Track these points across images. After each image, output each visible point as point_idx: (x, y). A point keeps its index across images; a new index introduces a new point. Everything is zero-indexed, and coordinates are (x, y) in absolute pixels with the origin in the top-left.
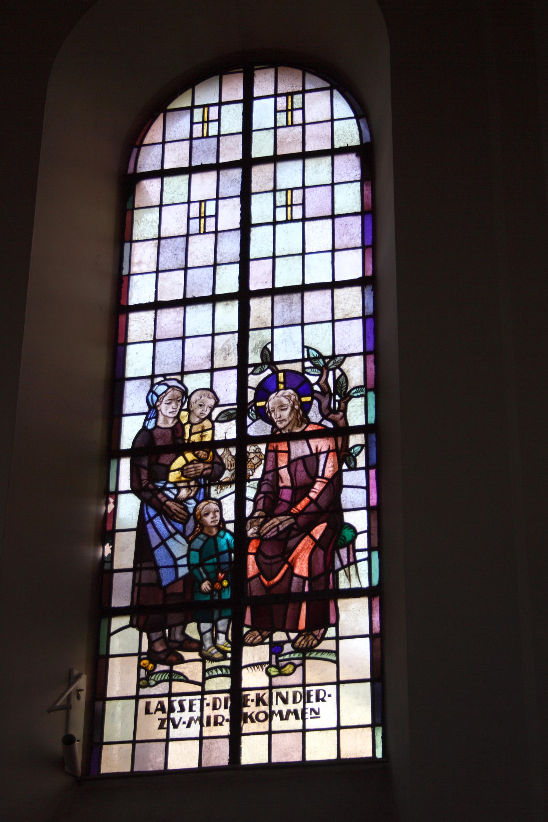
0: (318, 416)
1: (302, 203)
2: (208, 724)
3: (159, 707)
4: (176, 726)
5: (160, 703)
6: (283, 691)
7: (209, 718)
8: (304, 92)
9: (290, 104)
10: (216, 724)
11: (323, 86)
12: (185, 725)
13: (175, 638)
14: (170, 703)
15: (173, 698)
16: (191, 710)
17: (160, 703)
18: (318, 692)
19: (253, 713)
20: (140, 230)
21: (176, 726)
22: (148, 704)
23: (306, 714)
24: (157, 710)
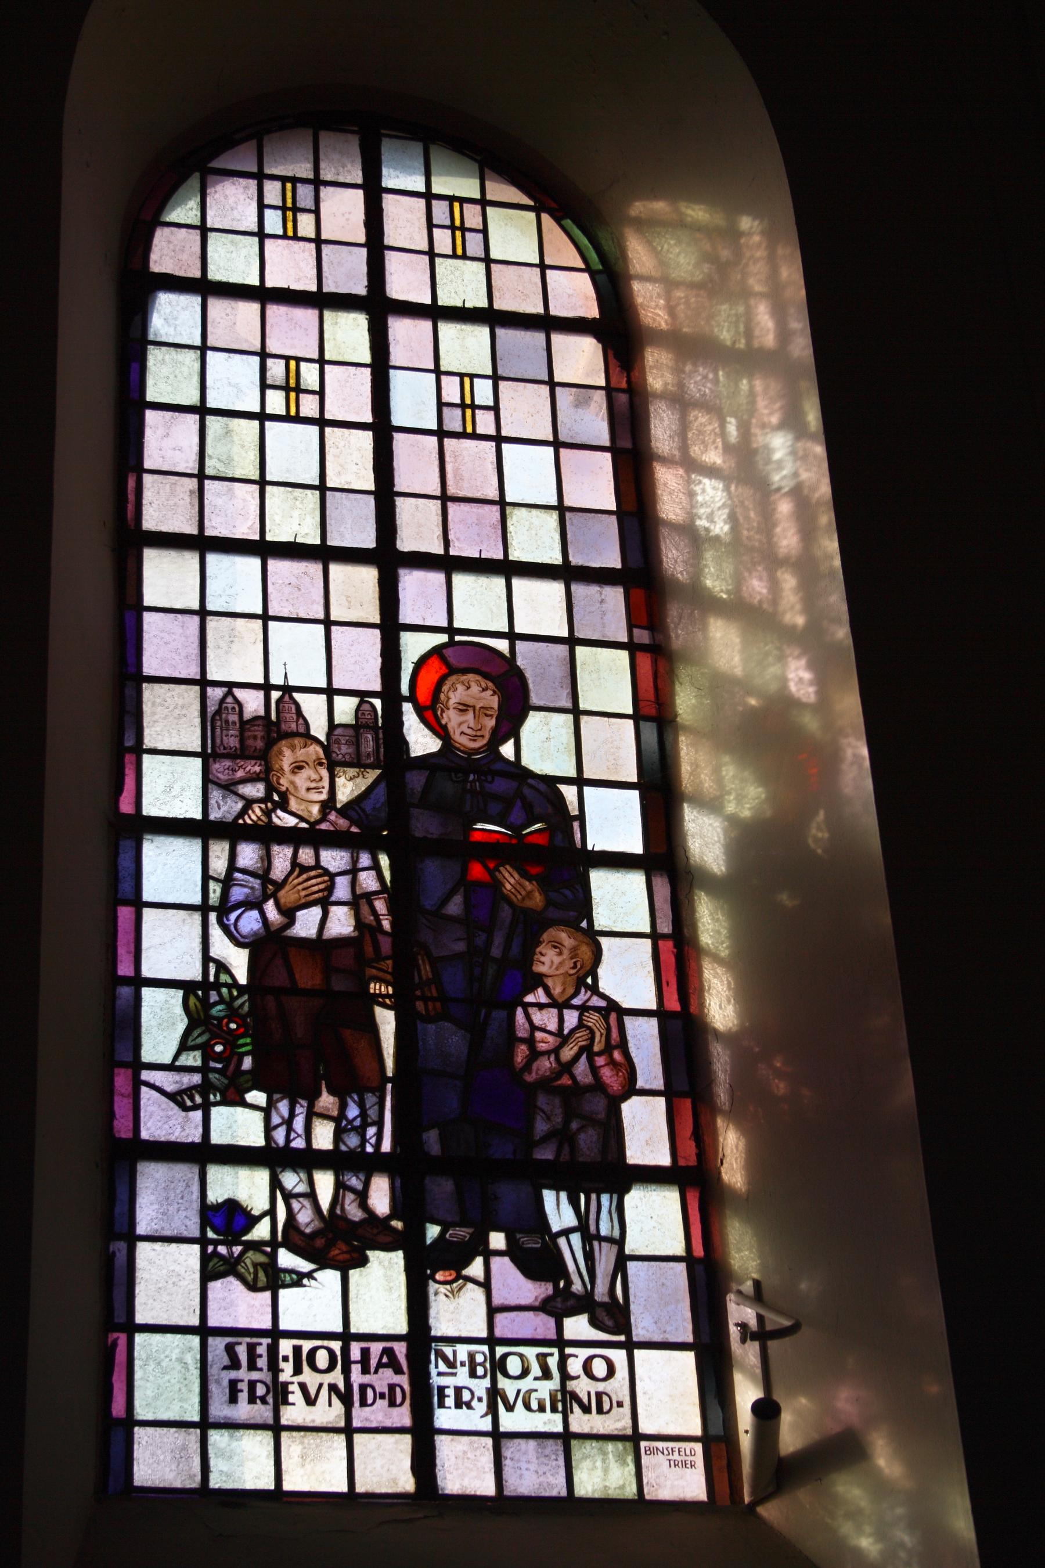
0: (700, 821)
1: (302, 415)
2: (363, 1403)
3: (385, 1360)
4: (510, 1408)
5: (388, 1352)
6: (448, 1351)
7: (363, 1388)
8: (483, 203)
9: (290, 225)
10: (459, 1404)
11: (515, 201)
12: (386, 1402)
13: (312, 1221)
14: (346, 1350)
15: (568, 1351)
16: (252, 1366)
17: (388, 1352)
18: (313, 1352)
19: (536, 1390)
20: (709, 385)
21: (510, 1408)
22: (365, 1353)
23: (447, 1399)
24: (380, 1365)
